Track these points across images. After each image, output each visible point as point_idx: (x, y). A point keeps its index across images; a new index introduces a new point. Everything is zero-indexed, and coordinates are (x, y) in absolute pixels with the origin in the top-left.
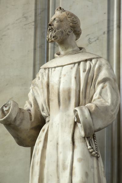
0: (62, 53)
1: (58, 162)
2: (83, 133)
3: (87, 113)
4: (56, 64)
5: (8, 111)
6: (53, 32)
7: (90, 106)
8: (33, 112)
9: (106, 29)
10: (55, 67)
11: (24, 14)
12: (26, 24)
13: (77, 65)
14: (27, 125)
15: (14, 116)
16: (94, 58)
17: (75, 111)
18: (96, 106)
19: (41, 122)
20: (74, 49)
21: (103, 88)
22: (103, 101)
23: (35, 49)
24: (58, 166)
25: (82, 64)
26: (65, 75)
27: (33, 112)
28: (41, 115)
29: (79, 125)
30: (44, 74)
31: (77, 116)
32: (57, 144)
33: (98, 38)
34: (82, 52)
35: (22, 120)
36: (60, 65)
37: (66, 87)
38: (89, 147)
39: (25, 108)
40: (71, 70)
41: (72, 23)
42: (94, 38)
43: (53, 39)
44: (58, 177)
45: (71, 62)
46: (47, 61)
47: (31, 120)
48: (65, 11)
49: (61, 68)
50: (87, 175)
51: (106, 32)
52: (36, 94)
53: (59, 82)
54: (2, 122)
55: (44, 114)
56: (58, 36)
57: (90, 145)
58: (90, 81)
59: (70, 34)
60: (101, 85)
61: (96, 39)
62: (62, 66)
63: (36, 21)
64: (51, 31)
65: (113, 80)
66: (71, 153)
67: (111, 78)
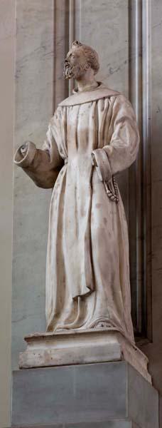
0: (80, 89)
1: (76, 207)
2: (101, 177)
3: (104, 157)
5: (25, 153)
7: (108, 149)
8: (51, 150)
9: (127, 59)
10: (73, 106)
11: (42, 44)
12: (45, 55)
13: (94, 103)
14: (45, 168)
15: (31, 159)
16: (112, 96)
17: (92, 154)
18: (114, 149)
19: (60, 163)
20: (92, 85)
21: (121, 128)
22: (122, 142)
23: (54, 81)
24: (76, 212)
25: (100, 102)
26: (82, 115)
27: (51, 150)
28: (60, 156)
29: (97, 169)
31: (94, 160)
32: (76, 188)
35: (40, 162)
37: (84, 127)
38: (108, 191)
39: (43, 149)
44: (77, 224)
45: (88, 100)
46: (66, 96)
47: (49, 161)
50: (105, 221)
51: (128, 62)
52: (54, 134)
54: (19, 165)
55: (62, 155)
56: (75, 73)
57: (109, 189)
58: (109, 120)
60: (119, 125)
62: (80, 104)
63: (55, 51)
65: (132, 119)
66: (89, 198)
67: (130, 117)
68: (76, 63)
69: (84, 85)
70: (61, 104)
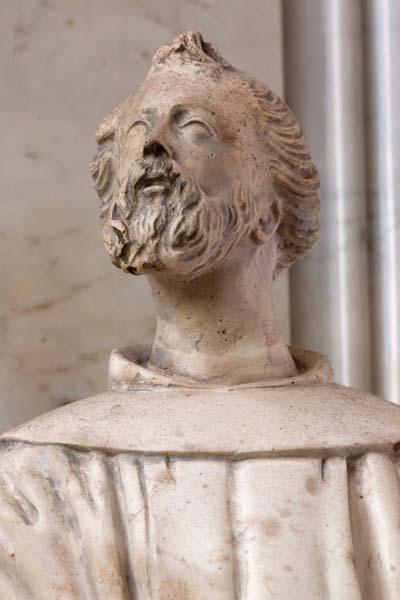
4: (179, 434)
6: (177, 200)
10: (168, 457)
13: (337, 468)
26: (270, 528)
30: (70, 488)
34: (316, 383)
36: (213, 446)
41: (292, 167)
45: (300, 442)
48: (228, 68)
49: (217, 468)
53: (227, 567)
59: (204, 240)
64: (153, 195)
68: (216, 177)
69: (226, 337)
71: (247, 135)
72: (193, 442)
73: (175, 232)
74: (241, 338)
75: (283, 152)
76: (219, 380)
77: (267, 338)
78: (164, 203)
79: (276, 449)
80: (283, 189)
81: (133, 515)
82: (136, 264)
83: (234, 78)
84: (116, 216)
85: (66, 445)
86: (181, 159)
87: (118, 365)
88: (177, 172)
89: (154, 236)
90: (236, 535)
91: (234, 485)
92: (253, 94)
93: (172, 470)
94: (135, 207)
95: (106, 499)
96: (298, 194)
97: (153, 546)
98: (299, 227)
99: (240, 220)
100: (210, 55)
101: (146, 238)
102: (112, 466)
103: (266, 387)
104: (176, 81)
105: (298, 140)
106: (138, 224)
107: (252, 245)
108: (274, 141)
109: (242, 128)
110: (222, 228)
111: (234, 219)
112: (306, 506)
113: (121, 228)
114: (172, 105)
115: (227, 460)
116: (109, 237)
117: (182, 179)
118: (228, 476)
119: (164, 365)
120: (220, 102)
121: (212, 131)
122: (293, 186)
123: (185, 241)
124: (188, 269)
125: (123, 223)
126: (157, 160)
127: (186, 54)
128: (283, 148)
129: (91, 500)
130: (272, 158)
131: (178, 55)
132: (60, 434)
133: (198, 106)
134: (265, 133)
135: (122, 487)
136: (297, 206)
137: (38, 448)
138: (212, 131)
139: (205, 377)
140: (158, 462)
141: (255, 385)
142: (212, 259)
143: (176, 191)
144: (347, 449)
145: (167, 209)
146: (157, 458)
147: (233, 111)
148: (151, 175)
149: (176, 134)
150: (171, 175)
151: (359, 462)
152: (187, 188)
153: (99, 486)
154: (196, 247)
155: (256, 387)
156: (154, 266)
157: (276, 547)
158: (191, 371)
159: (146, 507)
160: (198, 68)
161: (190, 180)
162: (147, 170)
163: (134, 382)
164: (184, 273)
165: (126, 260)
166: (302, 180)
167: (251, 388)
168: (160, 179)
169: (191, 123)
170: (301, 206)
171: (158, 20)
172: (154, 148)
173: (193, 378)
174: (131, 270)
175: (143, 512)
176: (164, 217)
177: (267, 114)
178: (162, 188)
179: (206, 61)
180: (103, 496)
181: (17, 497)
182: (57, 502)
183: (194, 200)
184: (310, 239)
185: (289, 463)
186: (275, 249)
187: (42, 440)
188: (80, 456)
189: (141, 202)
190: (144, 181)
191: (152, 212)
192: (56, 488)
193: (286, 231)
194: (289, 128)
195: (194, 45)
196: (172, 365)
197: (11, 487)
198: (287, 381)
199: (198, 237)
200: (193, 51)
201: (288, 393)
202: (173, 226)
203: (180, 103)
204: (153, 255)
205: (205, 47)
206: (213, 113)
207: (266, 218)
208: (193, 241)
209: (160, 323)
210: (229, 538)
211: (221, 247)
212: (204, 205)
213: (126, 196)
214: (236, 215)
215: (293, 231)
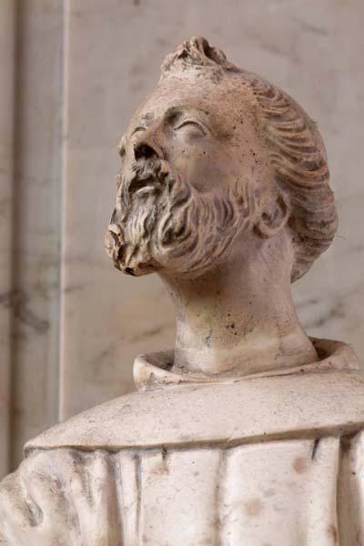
4: (176, 426)
6: (167, 199)
10: (165, 450)
13: (330, 447)
26: (253, 508)
30: (74, 486)
33: (340, 305)
36: (207, 435)
40: (297, 477)
41: (295, 160)
42: (314, 302)
43: (161, 252)
45: (292, 424)
48: (232, 70)
49: (210, 456)
59: (193, 235)
61: (323, 308)
62: (225, 445)
64: (145, 196)
68: (207, 174)
69: (235, 331)
70: (73, 431)
71: (245, 131)
72: (189, 432)
73: (164, 229)
74: (251, 331)
75: (283, 146)
76: (229, 373)
77: (279, 329)
78: (155, 203)
79: (267, 433)
80: (285, 182)
81: (126, 508)
82: (132, 265)
83: (235, 79)
84: (114, 220)
85: (73, 447)
86: (172, 159)
87: (139, 369)
88: (165, 171)
89: (145, 236)
90: (221, 518)
91: (225, 470)
92: (252, 92)
93: (168, 461)
94: (131, 209)
95: (103, 495)
96: (304, 187)
97: (141, 534)
98: (310, 220)
99: (238, 215)
100: (213, 59)
101: (138, 238)
102: (114, 463)
103: (291, 374)
104: (177, 85)
105: (299, 134)
106: (131, 225)
107: (257, 239)
108: (274, 137)
109: (239, 126)
110: (216, 223)
111: (230, 212)
112: (292, 485)
113: (117, 231)
114: (166, 109)
115: (221, 447)
116: (109, 241)
117: (170, 177)
118: (220, 462)
119: (182, 365)
120: (215, 103)
121: (206, 130)
122: (297, 179)
123: (175, 238)
124: (184, 264)
125: (119, 226)
126: (148, 161)
127: (189, 60)
128: (283, 142)
129: (90, 497)
130: (273, 153)
131: (181, 61)
132: (69, 437)
133: (192, 107)
134: (265, 129)
135: (121, 482)
136: (305, 199)
137: (50, 452)
138: (206, 130)
139: (216, 372)
140: (155, 455)
141: (261, 375)
142: (208, 254)
143: (166, 191)
144: (341, 428)
145: (157, 209)
146: (155, 451)
147: (230, 111)
148: (142, 177)
149: (170, 135)
150: (159, 175)
151: (354, 440)
152: (175, 186)
153: (98, 482)
154: (185, 242)
155: (268, 377)
156: (151, 266)
157: (257, 526)
158: (204, 367)
159: (139, 499)
160: (199, 71)
161: (179, 178)
162: (137, 172)
163: (150, 381)
164: (180, 270)
165: (124, 261)
166: (306, 172)
167: (256, 378)
168: (150, 180)
169: (185, 124)
170: (310, 198)
171: (275, 50)
172: (143, 150)
173: (205, 374)
174: (129, 271)
175: (135, 503)
176: (152, 216)
177: (266, 110)
178: (153, 188)
179: (208, 64)
180: (100, 492)
181: (29, 502)
182: (62, 502)
183: (183, 197)
184: (325, 230)
185: (260, 447)
186: (288, 241)
187: (52, 445)
188: (87, 456)
189: (136, 202)
190: (136, 184)
191: (143, 212)
192: (63, 489)
193: (298, 226)
194: (290, 123)
195: (196, 50)
196: (187, 363)
197: (25, 493)
198: (298, 369)
199: (186, 233)
200: (195, 56)
201: (295, 379)
202: (161, 223)
203: (174, 105)
204: (147, 254)
205: (208, 51)
206: (207, 113)
207: (271, 212)
208: (182, 237)
209: (179, 323)
210: (212, 519)
211: (217, 241)
212: (193, 201)
213: (122, 200)
214: (232, 210)
215: (304, 223)
